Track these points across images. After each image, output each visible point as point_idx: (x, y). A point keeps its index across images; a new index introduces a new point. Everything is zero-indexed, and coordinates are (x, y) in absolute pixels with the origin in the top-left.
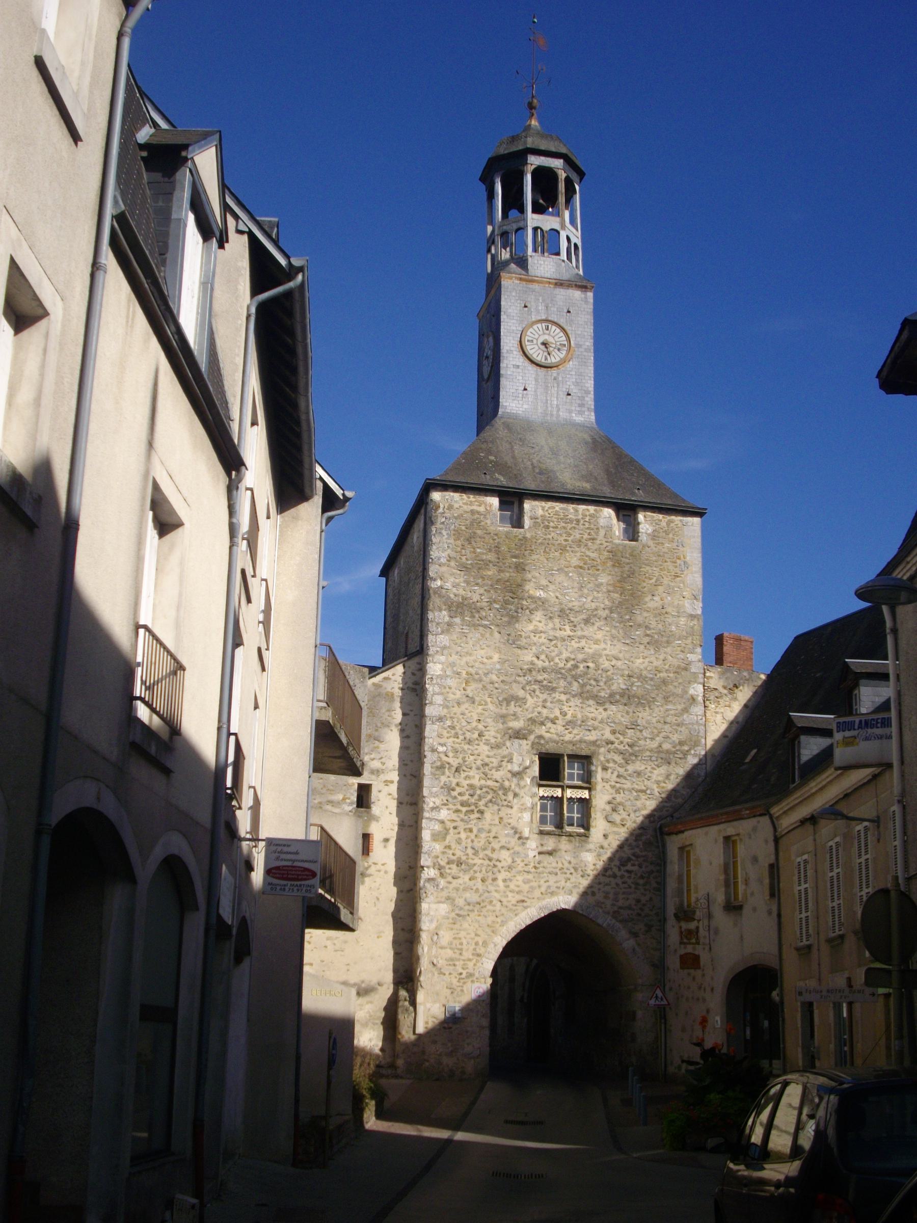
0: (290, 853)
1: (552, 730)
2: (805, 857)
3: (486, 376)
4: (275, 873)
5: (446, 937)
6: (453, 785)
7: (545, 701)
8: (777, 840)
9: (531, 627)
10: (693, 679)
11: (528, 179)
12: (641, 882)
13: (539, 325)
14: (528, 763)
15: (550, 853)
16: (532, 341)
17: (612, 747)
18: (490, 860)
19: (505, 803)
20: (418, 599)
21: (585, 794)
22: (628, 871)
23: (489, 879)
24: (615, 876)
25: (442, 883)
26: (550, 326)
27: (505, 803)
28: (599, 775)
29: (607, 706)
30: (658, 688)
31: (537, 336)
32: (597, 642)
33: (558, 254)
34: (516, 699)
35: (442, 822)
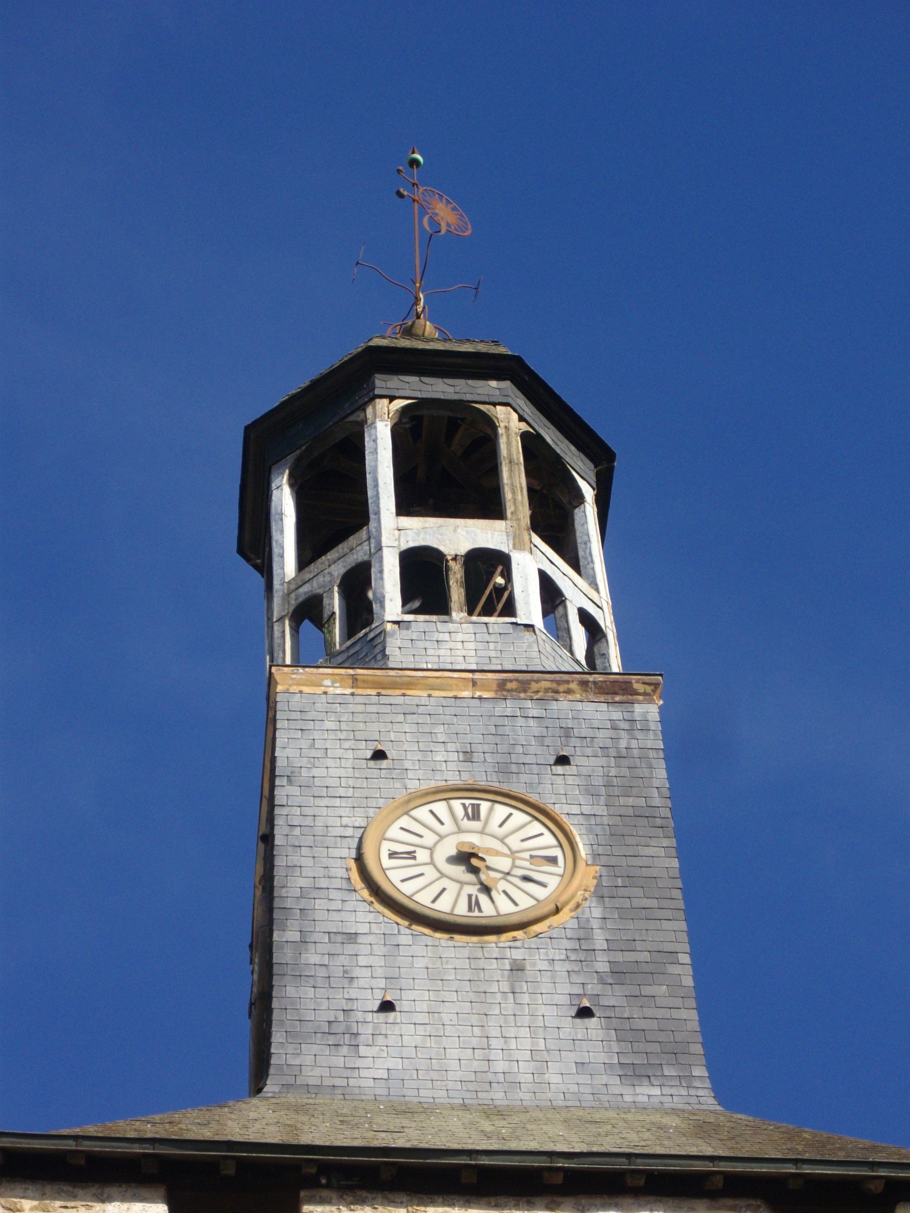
13: (440, 808)
16: (411, 855)
26: (485, 806)
31: (429, 839)
33: (509, 609)
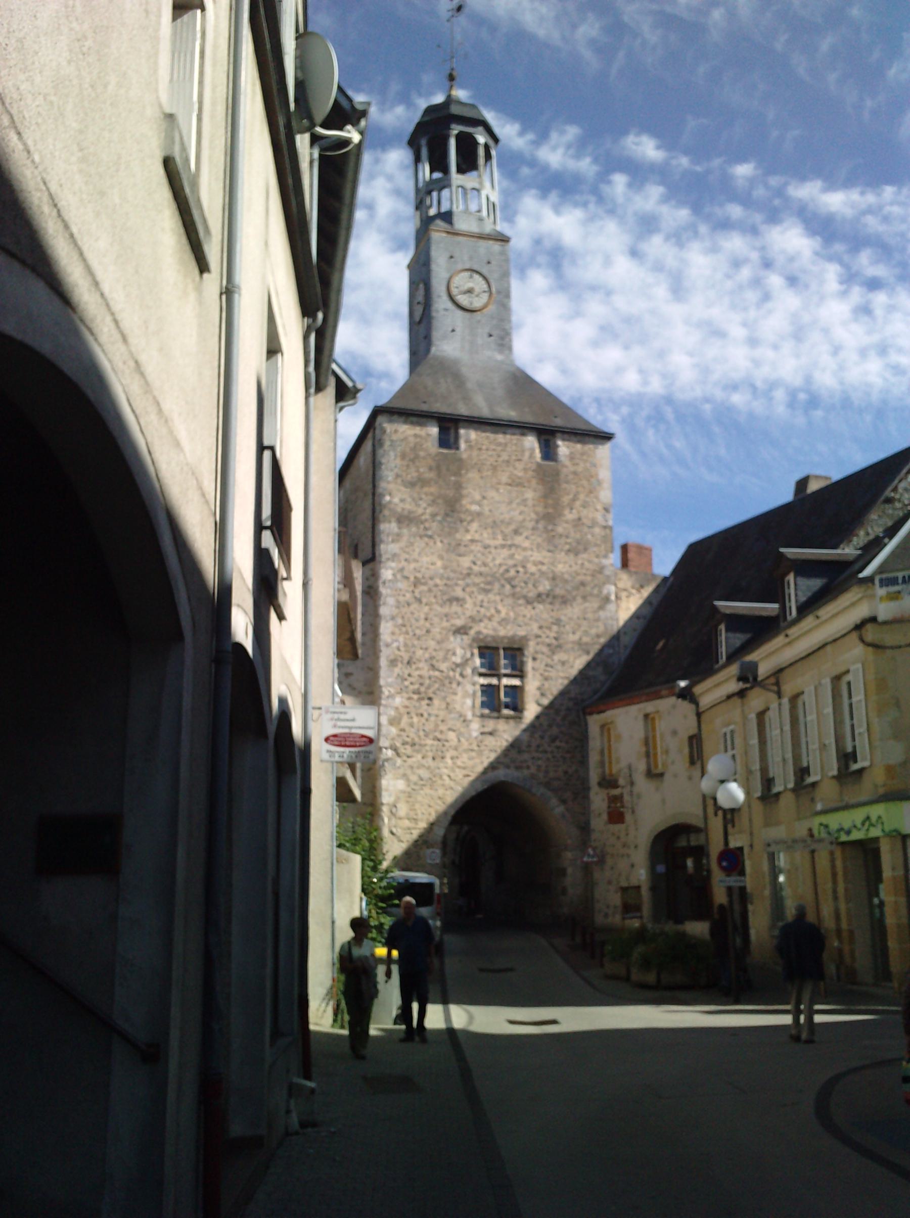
0: (347, 720)
1: (490, 626)
2: (732, 727)
3: (417, 319)
4: (332, 741)
5: (403, 809)
6: (406, 676)
7: (482, 601)
8: (699, 715)
9: (469, 537)
10: (608, 580)
11: (452, 143)
12: (568, 756)
14: (468, 655)
15: (491, 734)
17: (539, 640)
18: (439, 740)
19: (451, 691)
20: (368, 513)
21: (516, 682)
22: (558, 748)
23: (438, 757)
24: (545, 752)
25: (399, 761)
27: (451, 691)
28: (529, 665)
29: (536, 604)
30: (577, 588)
32: (525, 549)
34: (457, 599)
35: (397, 708)
